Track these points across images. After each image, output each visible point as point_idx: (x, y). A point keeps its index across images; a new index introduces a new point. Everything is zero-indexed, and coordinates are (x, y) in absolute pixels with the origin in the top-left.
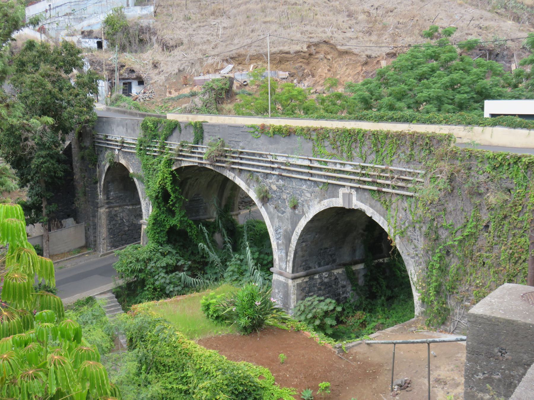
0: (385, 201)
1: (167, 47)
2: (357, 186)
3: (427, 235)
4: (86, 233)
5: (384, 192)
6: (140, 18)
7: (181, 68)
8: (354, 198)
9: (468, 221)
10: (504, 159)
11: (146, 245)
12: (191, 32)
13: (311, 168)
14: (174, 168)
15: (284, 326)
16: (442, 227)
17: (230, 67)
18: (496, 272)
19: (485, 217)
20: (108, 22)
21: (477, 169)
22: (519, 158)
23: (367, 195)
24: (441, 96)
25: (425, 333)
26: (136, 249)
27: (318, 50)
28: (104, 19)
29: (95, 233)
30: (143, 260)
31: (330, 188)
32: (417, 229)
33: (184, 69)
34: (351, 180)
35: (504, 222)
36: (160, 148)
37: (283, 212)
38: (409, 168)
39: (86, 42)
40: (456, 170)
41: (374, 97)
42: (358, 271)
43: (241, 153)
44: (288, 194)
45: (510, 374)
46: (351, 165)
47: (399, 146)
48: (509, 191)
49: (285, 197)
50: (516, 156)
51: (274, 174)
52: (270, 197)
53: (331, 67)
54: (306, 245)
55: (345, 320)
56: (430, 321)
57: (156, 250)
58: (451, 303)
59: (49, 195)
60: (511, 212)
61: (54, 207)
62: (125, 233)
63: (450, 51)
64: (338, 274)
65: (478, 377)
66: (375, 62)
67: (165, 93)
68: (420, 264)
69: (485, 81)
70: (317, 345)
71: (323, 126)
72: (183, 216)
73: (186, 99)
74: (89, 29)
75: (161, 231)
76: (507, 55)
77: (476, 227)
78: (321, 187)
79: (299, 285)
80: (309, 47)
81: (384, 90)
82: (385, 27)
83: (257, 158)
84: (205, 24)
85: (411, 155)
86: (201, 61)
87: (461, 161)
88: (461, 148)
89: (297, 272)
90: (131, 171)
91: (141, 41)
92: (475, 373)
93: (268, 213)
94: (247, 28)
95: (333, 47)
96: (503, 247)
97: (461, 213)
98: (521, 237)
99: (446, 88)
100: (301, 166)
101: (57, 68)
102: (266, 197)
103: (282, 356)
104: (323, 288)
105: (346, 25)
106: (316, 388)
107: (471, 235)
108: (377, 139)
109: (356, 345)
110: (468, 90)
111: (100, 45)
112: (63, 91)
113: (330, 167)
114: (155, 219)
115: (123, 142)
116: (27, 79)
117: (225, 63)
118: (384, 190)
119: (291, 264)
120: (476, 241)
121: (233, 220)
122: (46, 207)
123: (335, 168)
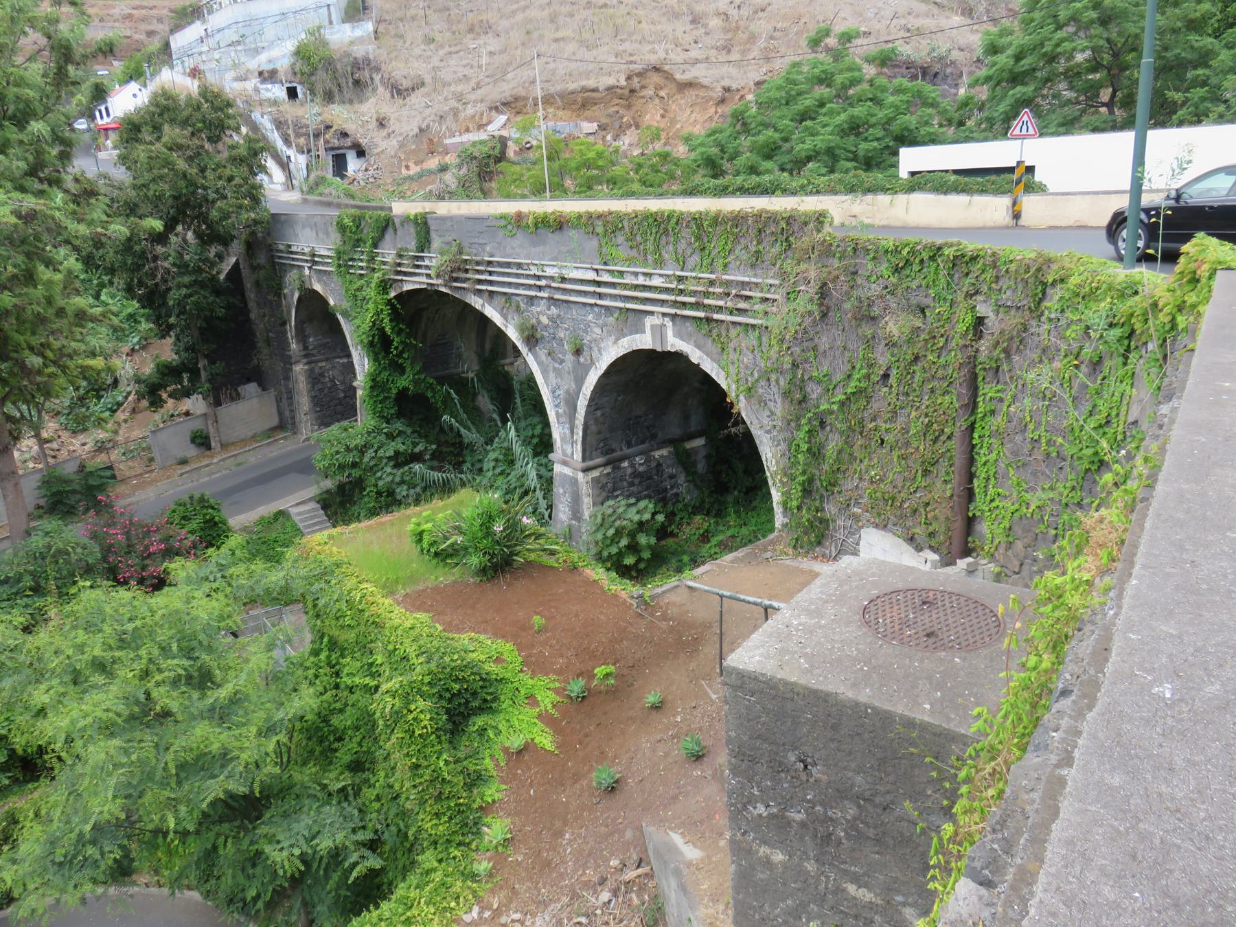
0: (719, 335)
1: (398, 91)
2: (673, 311)
3: (786, 394)
5: (717, 321)
6: (352, 43)
7: (424, 126)
8: (670, 333)
9: (854, 367)
10: (912, 252)
11: (365, 420)
13: (599, 284)
14: (393, 294)
15: (551, 561)
18: (902, 457)
19: (883, 359)
22: (939, 249)
24: (833, 148)
25: (788, 562)
26: (346, 430)
27: (643, 82)
28: (293, 49)
29: (291, 404)
30: (356, 447)
31: (631, 316)
32: (774, 383)
33: (428, 127)
34: (663, 303)
36: (368, 261)
37: (562, 362)
38: (755, 276)
39: (267, 90)
40: (831, 277)
41: (726, 156)
42: (695, 451)
43: (490, 263)
44: (566, 329)
45: (826, 816)
46: (661, 275)
47: (737, 238)
48: (923, 311)
49: (562, 335)
51: (542, 298)
52: (538, 336)
53: (666, 111)
56: (797, 540)
57: (378, 430)
58: (831, 509)
60: (927, 350)
61: (219, 367)
63: (850, 69)
64: (662, 456)
65: (756, 812)
66: (737, 98)
67: (400, 168)
68: (778, 445)
69: (907, 117)
70: (603, 592)
71: (613, 209)
74: (270, 67)
75: (386, 398)
76: (952, 74)
77: (867, 377)
78: (616, 315)
79: (595, 481)
80: (629, 78)
81: (745, 142)
82: (753, 38)
84: (458, 48)
86: (455, 113)
87: (840, 259)
89: (592, 459)
90: (332, 303)
91: (357, 83)
92: (749, 802)
94: (527, 52)
95: (669, 77)
96: (914, 414)
97: (842, 353)
98: (944, 395)
100: (582, 282)
101: (193, 134)
102: (533, 336)
103: (537, 620)
104: (637, 481)
105: (690, 38)
107: (859, 392)
110: (881, 134)
111: (292, 93)
113: (629, 280)
114: (373, 380)
115: (314, 255)
116: (141, 152)
117: (494, 113)
119: (579, 447)
120: (868, 403)
122: (205, 368)
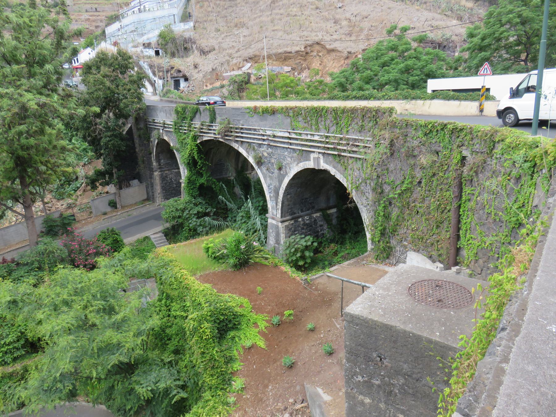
0: (344, 162)
1: (203, 52)
2: (323, 151)
3: (374, 190)
4: (147, 190)
5: (343, 156)
6: (184, 31)
7: (214, 68)
8: (322, 161)
9: (405, 178)
10: (433, 126)
11: (185, 197)
12: (221, 41)
13: (290, 138)
14: (198, 142)
15: (266, 262)
16: (385, 183)
17: (249, 65)
18: (427, 220)
19: (419, 174)
20: (162, 36)
21: (412, 136)
22: (446, 125)
23: (330, 158)
24: (398, 79)
25: (373, 266)
26: (176, 201)
27: (312, 49)
28: (158, 34)
29: (152, 189)
33: (216, 68)
34: (319, 147)
35: (433, 179)
36: (188, 127)
37: (273, 173)
39: (146, 52)
41: (349, 82)
42: (332, 214)
43: (242, 129)
44: (275, 159)
46: (318, 135)
47: (353, 119)
48: (437, 153)
49: (273, 161)
50: (443, 123)
51: (265, 144)
52: (263, 161)
53: (322, 62)
54: (291, 197)
55: (322, 250)
56: (378, 256)
58: (393, 242)
59: (116, 164)
60: (439, 171)
61: (122, 172)
62: (171, 190)
63: (406, 44)
64: (317, 216)
65: (357, 380)
66: (354, 56)
69: (432, 66)
71: (297, 105)
72: (209, 177)
73: (217, 90)
74: (148, 42)
75: (194, 187)
76: (452, 46)
78: (297, 153)
80: (305, 47)
81: (357, 76)
82: (361, 30)
83: (253, 132)
84: (230, 34)
85: (362, 125)
86: (228, 62)
87: (400, 129)
88: (400, 118)
90: (172, 145)
91: (186, 49)
92: (354, 375)
93: (262, 174)
94: (261, 36)
95: (323, 47)
96: (432, 200)
99: (402, 72)
100: (283, 137)
103: (259, 289)
104: (305, 227)
105: (333, 30)
106: (283, 315)
107: (408, 189)
108: (336, 114)
109: (319, 277)
110: (419, 73)
111: (157, 53)
112: (119, 88)
113: (304, 137)
114: (189, 179)
115: (165, 124)
116: (91, 78)
117: (245, 62)
118: (343, 154)
119: (280, 211)
121: (248, 177)
123: (307, 138)
